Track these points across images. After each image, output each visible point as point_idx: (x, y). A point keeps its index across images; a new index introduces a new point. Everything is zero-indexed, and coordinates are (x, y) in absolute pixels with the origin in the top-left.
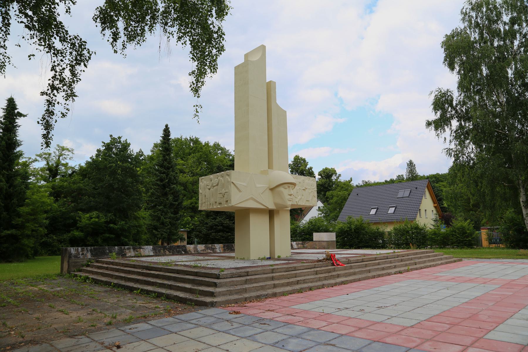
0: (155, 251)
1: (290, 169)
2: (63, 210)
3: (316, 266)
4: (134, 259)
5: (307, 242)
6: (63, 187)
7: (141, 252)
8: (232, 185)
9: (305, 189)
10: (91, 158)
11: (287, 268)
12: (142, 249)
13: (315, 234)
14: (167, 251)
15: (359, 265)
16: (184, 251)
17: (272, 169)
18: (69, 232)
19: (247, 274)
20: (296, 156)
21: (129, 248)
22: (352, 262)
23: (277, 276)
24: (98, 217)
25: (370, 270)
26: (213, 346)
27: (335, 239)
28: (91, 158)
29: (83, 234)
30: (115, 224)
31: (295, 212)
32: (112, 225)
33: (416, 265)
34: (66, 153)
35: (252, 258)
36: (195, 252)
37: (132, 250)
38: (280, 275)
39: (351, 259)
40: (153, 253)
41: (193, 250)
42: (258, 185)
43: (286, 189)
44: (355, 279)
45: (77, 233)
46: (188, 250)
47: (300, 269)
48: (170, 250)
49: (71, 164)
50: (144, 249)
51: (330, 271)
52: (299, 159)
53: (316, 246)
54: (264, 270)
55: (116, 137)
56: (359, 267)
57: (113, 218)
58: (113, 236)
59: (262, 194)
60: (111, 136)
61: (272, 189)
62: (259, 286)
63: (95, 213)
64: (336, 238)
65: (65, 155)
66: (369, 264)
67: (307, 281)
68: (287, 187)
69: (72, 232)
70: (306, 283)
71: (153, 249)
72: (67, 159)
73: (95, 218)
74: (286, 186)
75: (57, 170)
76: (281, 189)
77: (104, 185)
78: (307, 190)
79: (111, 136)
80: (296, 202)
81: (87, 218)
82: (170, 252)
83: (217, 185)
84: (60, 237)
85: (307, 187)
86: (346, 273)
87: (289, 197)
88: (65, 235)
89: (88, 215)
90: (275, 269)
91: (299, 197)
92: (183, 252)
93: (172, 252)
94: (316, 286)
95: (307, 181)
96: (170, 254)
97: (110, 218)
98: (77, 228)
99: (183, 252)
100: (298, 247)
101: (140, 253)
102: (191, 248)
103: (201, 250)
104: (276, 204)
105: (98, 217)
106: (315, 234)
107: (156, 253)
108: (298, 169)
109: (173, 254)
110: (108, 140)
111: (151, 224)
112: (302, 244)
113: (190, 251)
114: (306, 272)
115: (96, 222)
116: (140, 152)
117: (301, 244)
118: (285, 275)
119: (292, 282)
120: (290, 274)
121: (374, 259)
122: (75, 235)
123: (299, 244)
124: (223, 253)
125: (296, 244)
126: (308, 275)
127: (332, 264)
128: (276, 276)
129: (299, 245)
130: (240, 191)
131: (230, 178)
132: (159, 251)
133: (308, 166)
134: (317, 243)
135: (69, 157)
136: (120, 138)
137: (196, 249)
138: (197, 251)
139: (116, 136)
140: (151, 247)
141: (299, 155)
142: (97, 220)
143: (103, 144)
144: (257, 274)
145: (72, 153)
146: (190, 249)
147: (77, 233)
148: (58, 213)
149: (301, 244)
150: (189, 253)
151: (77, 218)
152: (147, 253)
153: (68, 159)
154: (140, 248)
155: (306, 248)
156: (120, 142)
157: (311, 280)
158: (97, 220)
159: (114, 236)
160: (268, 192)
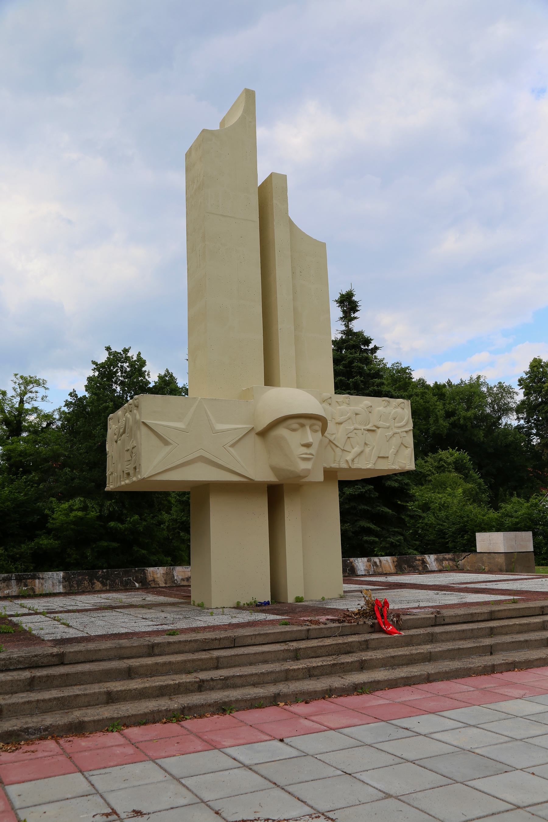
0: (70, 583)
1: (524, 390)
2: (21, 497)
3: (312, 634)
4: (163, 590)
5: (464, 555)
6: (26, 454)
7: (35, 586)
8: (144, 430)
9: (374, 428)
10: (70, 394)
11: (205, 641)
12: (39, 578)
13: (479, 536)
14: (99, 583)
15: (463, 631)
16: (141, 582)
17: (277, 385)
18: (31, 539)
19: (234, 643)
20: (535, 360)
21: (7, 578)
22: (447, 621)
23: (147, 665)
24: (85, 508)
25: (491, 646)
26: (408, 761)
27: (532, 549)
28: (70, 394)
29: (59, 542)
30: (122, 522)
31: (538, 481)
32: (112, 524)
33: (491, 654)
34: (34, 390)
35: (216, 602)
36: (166, 583)
37: (13, 582)
38: (157, 664)
39: (446, 612)
40: (64, 587)
41: (163, 580)
42: (219, 427)
43: (294, 430)
44: (407, 678)
45: (45, 542)
46: (150, 578)
47: (252, 642)
48: (107, 580)
49: (47, 408)
50: (43, 579)
51: (349, 649)
52: (542, 367)
53: (483, 565)
54: (121, 648)
55: (120, 350)
56: (463, 636)
57: (114, 509)
58: (115, 545)
59: (233, 446)
60: (108, 349)
61: (263, 434)
62: (50, 700)
63: (77, 502)
64: (534, 547)
65: (31, 392)
66: (502, 627)
67: (238, 681)
68: (295, 426)
69: (36, 540)
70: (235, 687)
71: (64, 578)
72: (38, 399)
73: (78, 510)
74: (293, 423)
75: (19, 422)
76: (282, 431)
77: (95, 444)
78: (379, 431)
79: (108, 349)
80: (347, 461)
81: (65, 510)
82: (104, 584)
83: (124, 432)
84: (15, 550)
85: (381, 423)
86: (393, 657)
87: (304, 450)
88: (23, 545)
89: (65, 505)
90: (158, 644)
91: (357, 449)
92: (137, 585)
93: (110, 585)
94: (246, 701)
95: (381, 408)
96: (104, 589)
97: (109, 510)
98: (49, 532)
99: (137, 585)
100: (440, 568)
101: (33, 589)
102: (159, 575)
103: (183, 580)
104: (274, 469)
105: (85, 508)
106: (479, 536)
107: (71, 586)
108: (540, 387)
109: (113, 589)
110: (103, 357)
111: (176, 520)
112: (453, 560)
113: (154, 580)
114: (255, 654)
115: (81, 519)
116: (165, 375)
117: (450, 559)
118: (178, 662)
119: (179, 685)
120: (193, 661)
121: (303, 636)
122: (41, 545)
123: (445, 559)
124: (396, 574)
125: (437, 560)
126: (265, 662)
127: (372, 626)
128: (142, 666)
129: (445, 563)
130: (166, 443)
131: (140, 414)
132: (79, 583)
133: (107, 359)
134: (485, 558)
135: (40, 395)
136: (126, 351)
137: (169, 576)
138: (173, 582)
139: (117, 348)
140: (61, 574)
141: (541, 358)
142: (80, 514)
143: (94, 366)
144: (94, 658)
145: (43, 387)
146: (155, 576)
147: (45, 542)
148: (9, 503)
149: (450, 559)
150: (153, 585)
151: (47, 512)
152: (48, 587)
153: (39, 399)
154: (34, 578)
155: (461, 570)
156: (127, 359)
157: (255, 679)
158: (80, 514)
159: (119, 544)
160: (253, 441)
